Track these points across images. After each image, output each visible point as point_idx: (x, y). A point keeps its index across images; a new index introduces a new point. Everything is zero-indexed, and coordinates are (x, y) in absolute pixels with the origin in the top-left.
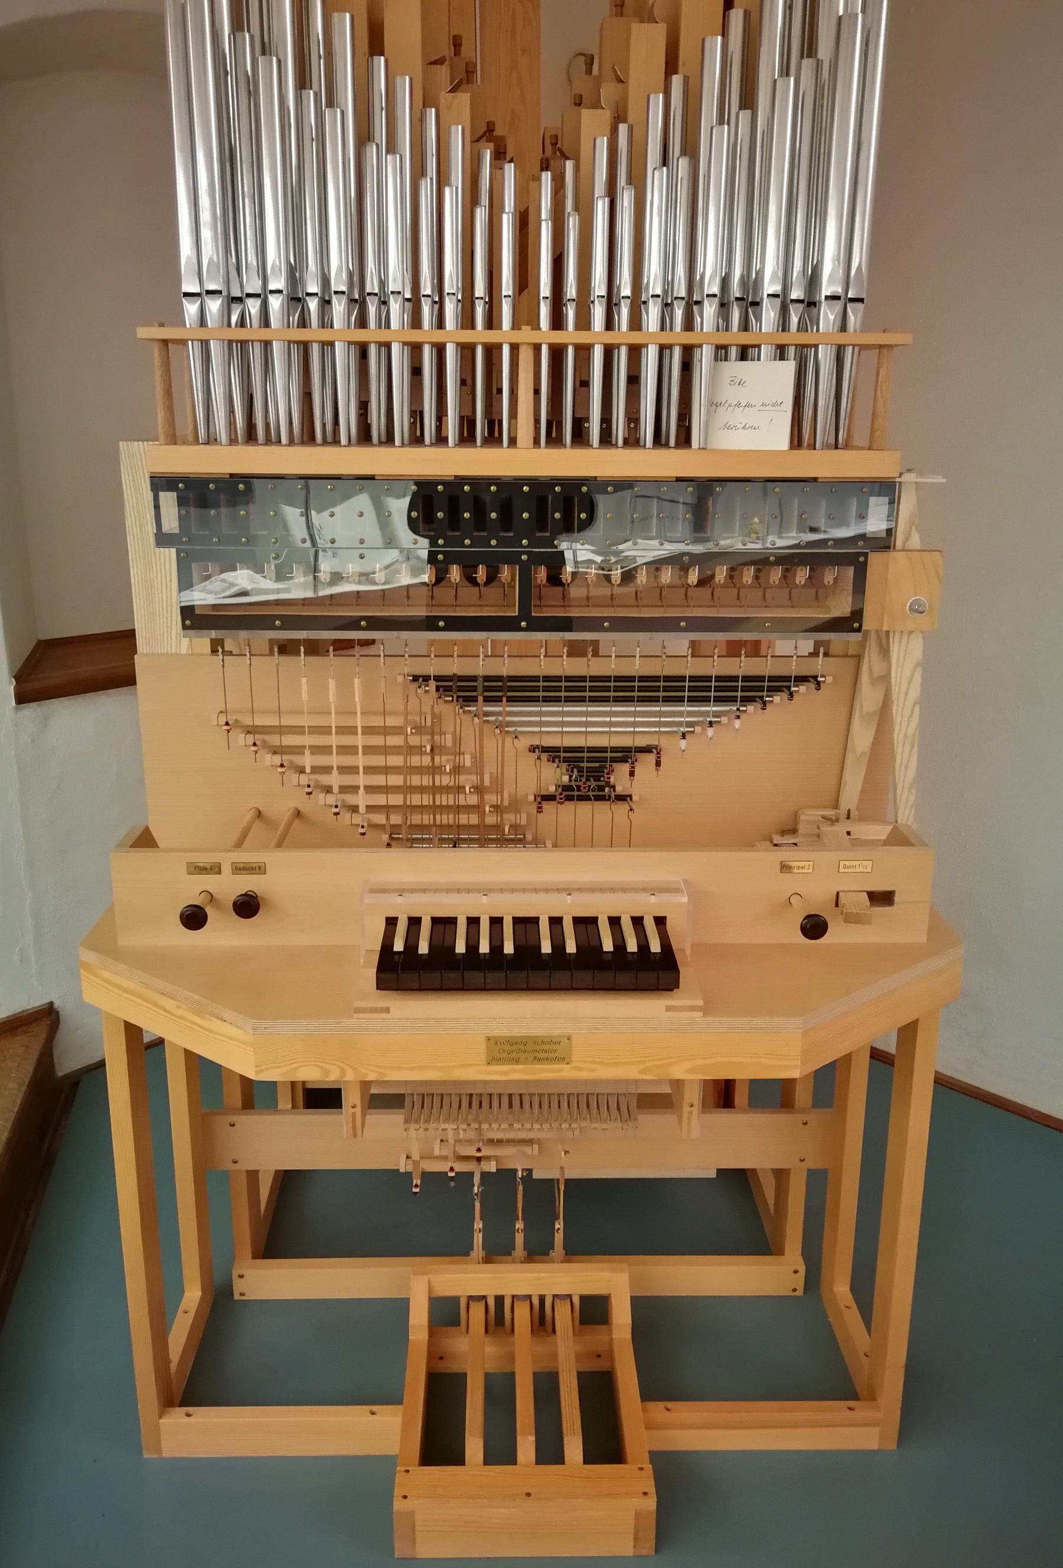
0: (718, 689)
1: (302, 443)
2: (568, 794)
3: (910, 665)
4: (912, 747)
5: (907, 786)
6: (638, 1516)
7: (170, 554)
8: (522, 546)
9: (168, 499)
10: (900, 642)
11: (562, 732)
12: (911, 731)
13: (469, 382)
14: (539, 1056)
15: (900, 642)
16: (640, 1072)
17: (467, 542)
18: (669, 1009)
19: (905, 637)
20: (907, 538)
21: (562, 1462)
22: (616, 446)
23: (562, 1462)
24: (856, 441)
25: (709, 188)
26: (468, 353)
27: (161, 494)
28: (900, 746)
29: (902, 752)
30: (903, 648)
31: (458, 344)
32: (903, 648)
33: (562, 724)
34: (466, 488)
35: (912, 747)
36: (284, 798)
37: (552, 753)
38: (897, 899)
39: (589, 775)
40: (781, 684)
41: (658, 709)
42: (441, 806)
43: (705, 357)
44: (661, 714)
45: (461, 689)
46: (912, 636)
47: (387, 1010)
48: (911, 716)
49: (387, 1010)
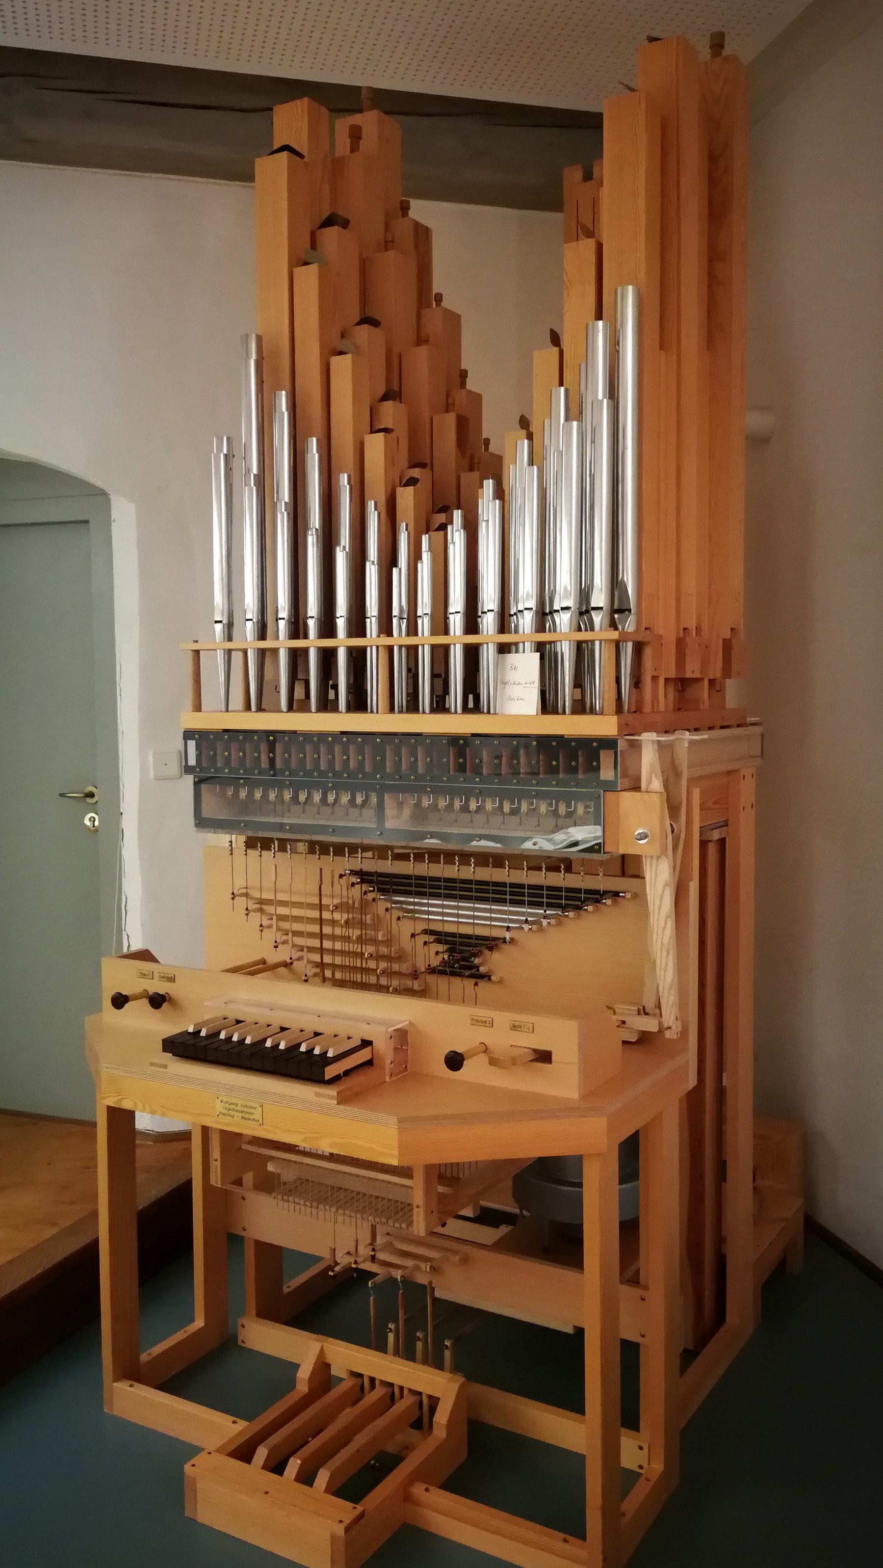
0: (549, 897)
1: (409, 711)
2: (445, 970)
3: (660, 886)
4: (668, 954)
5: (667, 987)
6: (333, 1537)
7: (190, 779)
8: (377, 779)
9: (192, 744)
10: (651, 865)
11: (458, 922)
12: (666, 941)
13: (413, 671)
14: (246, 1116)
15: (651, 865)
16: (303, 1141)
17: (287, 773)
18: (317, 1095)
19: (654, 862)
20: (649, 782)
21: (311, 1485)
22: (483, 713)
23: (311, 1485)
24: (605, 711)
25: (593, 527)
26: (412, 651)
27: (189, 741)
28: (659, 952)
29: (661, 957)
30: (654, 870)
31: (319, 648)
32: (654, 870)
33: (474, 917)
34: (595, 744)
35: (668, 954)
36: (262, 948)
37: (440, 937)
38: (554, 1058)
39: (463, 959)
40: (596, 897)
41: (524, 910)
42: (353, 967)
43: (488, 654)
44: (443, 907)
45: (379, 883)
46: (660, 861)
47: (165, 1067)
48: (664, 928)
49: (165, 1067)
